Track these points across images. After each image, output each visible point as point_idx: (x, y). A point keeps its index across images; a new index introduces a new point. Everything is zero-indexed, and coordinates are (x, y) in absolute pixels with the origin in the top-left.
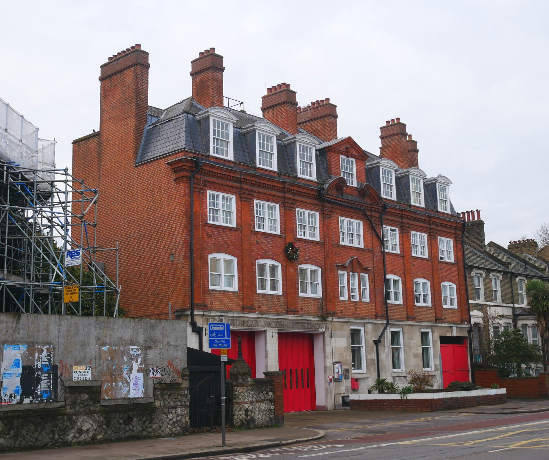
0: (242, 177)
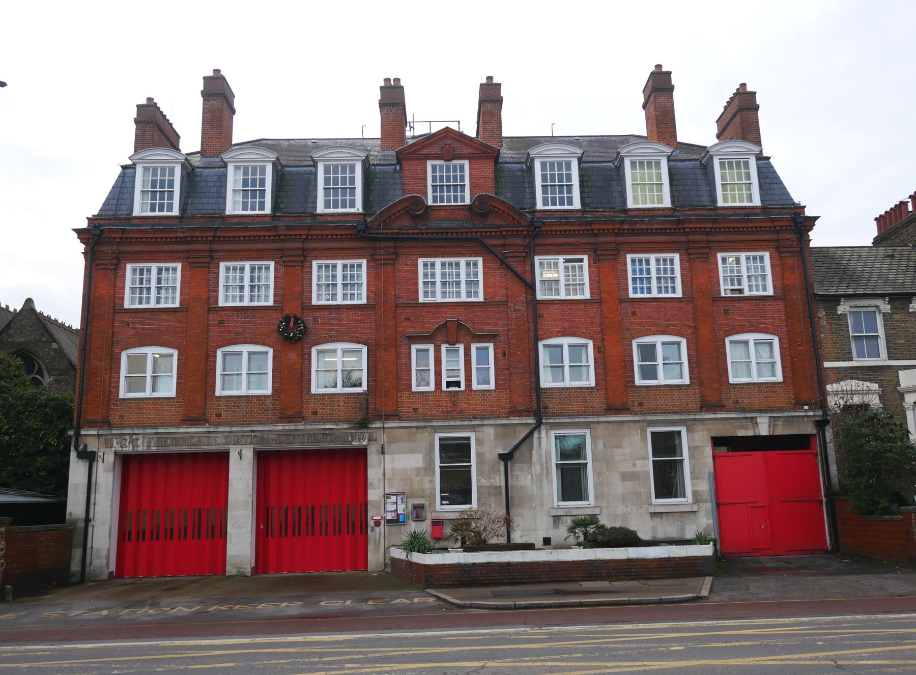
0: (186, 235)
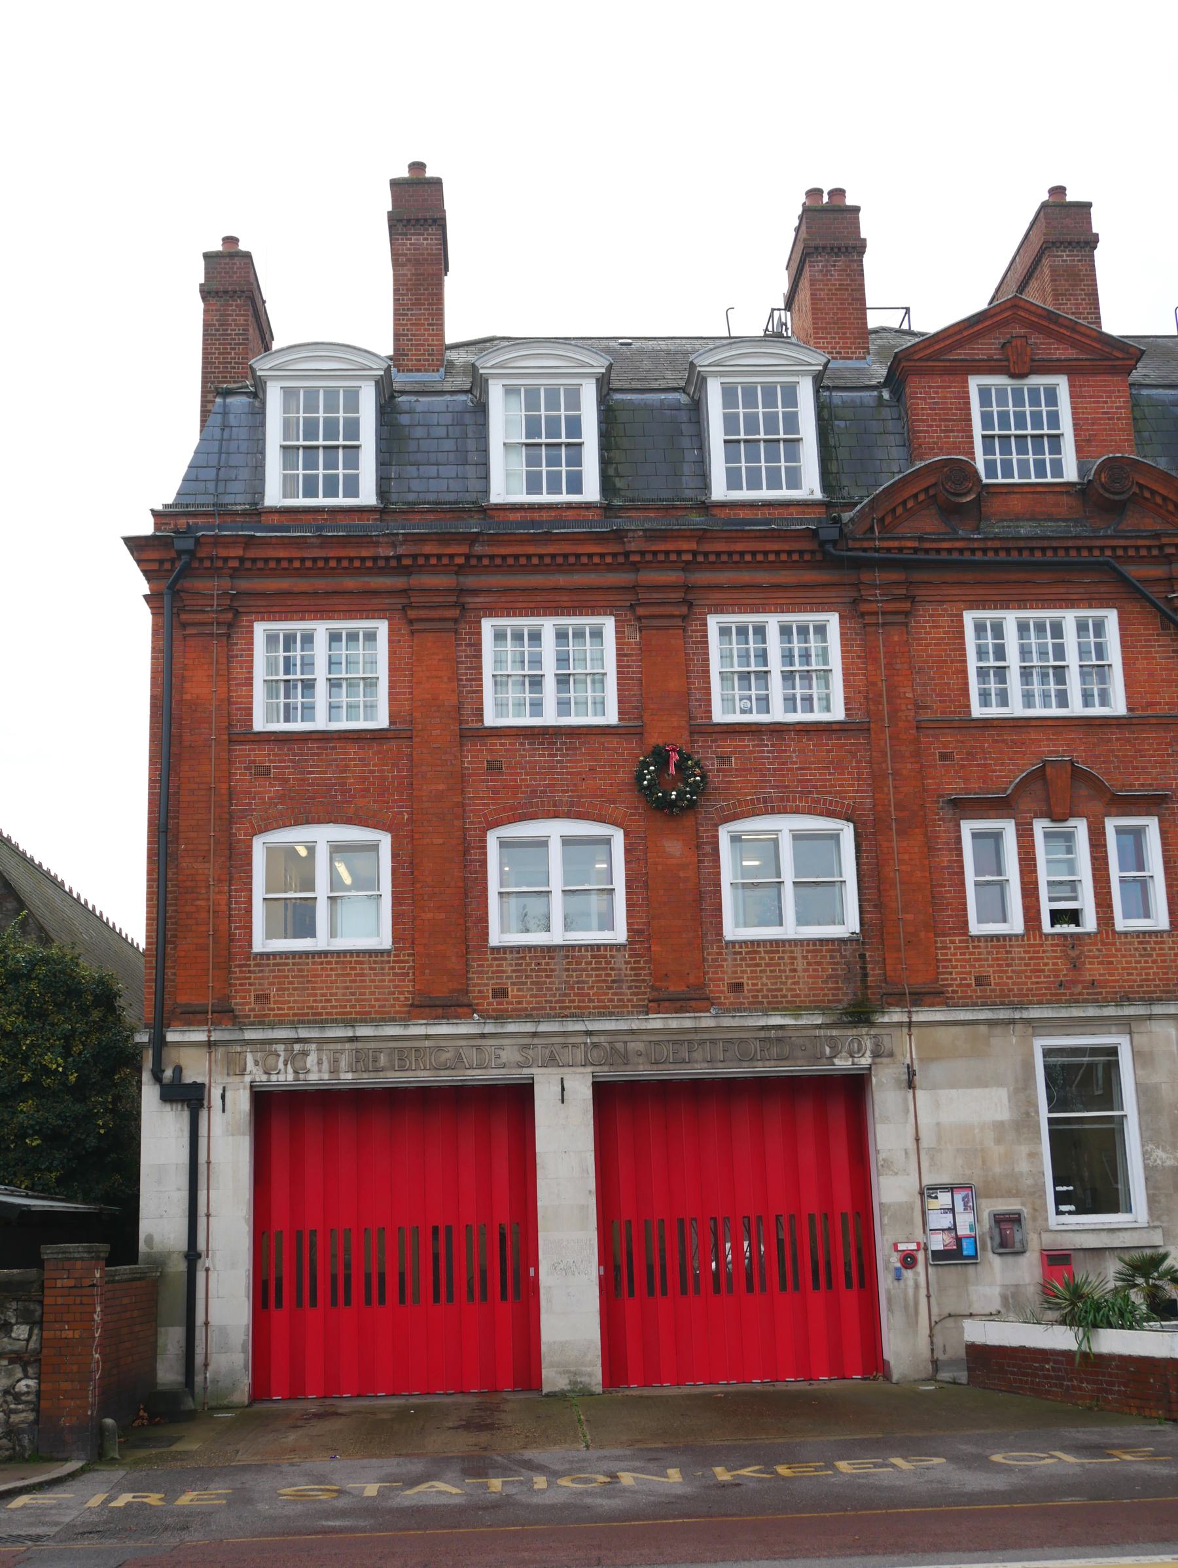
0: (401, 550)
